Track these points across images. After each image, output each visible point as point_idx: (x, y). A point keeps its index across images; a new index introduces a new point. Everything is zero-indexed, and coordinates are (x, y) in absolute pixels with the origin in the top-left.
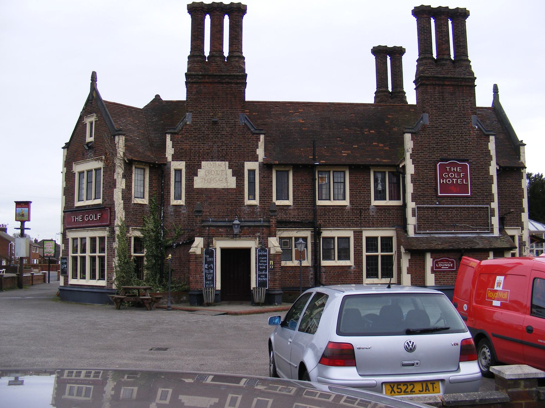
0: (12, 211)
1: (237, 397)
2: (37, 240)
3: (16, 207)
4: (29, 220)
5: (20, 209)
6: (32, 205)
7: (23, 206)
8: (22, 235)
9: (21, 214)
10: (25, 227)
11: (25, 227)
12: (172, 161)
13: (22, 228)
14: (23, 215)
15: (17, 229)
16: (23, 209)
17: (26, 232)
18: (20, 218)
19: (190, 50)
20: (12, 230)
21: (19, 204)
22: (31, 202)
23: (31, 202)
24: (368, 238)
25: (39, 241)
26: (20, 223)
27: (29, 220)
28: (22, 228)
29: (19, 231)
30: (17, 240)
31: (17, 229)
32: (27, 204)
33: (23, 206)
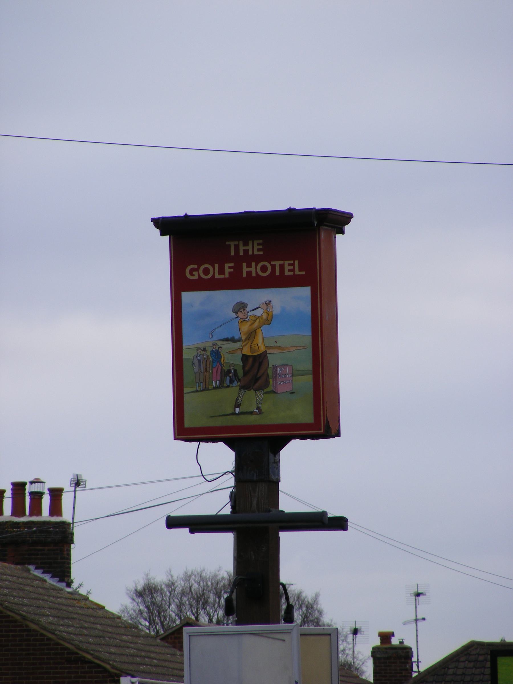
0: (124, 341)
1: (31, 493)
2: (405, 654)
3: (180, 284)
4: (324, 425)
5: (224, 300)
6: (347, 247)
7: (254, 283)
8: (256, 593)
9: (232, 358)
10: (288, 504)
11: (288, 504)
12: (44, 493)
13: (256, 521)
14: (254, 372)
15: (198, 524)
16: (255, 298)
17: (299, 560)
18: (220, 402)
19: (318, 207)
20: (139, 526)
21: (205, 248)
22: (336, 221)
23: (336, 221)
24: (31, 493)
25: (425, 659)
26: (220, 457)
27: (324, 425)
28: (256, 521)
29: (217, 556)
30: (197, 649)
31: (198, 524)
32: (296, 244)
33: (254, 283)
